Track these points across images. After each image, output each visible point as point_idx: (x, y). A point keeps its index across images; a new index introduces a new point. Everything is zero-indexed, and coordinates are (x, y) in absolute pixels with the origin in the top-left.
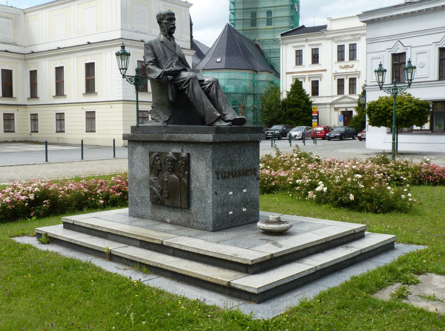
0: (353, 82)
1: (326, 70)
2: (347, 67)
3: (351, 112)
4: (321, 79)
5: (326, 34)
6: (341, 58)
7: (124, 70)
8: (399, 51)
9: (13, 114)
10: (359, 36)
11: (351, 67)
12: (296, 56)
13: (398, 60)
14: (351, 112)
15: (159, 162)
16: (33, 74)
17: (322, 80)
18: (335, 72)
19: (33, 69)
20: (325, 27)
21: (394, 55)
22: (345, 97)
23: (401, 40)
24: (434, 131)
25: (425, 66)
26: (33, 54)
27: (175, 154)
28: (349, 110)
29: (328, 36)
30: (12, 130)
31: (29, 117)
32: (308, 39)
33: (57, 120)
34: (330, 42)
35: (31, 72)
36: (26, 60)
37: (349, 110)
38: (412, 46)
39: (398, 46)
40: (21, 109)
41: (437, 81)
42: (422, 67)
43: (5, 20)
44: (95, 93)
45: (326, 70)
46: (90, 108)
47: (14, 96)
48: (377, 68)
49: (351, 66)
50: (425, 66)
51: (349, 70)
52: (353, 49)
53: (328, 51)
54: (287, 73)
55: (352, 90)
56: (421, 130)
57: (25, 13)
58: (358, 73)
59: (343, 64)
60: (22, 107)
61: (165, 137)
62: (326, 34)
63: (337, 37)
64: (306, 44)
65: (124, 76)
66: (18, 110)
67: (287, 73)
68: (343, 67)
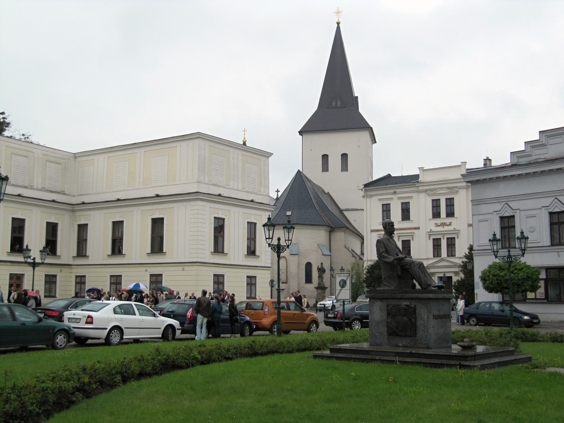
0: (451, 243)
1: (419, 228)
2: (443, 224)
3: (450, 278)
4: (413, 238)
5: (418, 186)
6: (436, 214)
7: (270, 240)
8: (507, 214)
9: (55, 276)
10: (457, 189)
11: (448, 225)
12: (383, 211)
13: (507, 223)
14: (450, 278)
15: (394, 311)
16: (82, 229)
17: (415, 238)
18: (429, 231)
19: (83, 222)
20: (417, 176)
21: (502, 218)
22: (443, 260)
23: (509, 203)
24: (550, 299)
25: (535, 227)
26: (82, 205)
27: (406, 305)
28: (448, 275)
29: (420, 188)
30: (53, 294)
31: (74, 279)
32: (397, 191)
33: (111, 283)
34: (423, 195)
35: (114, 223)
36: (73, 211)
37: (448, 275)
38: (521, 208)
39: (506, 209)
40: (65, 269)
41: (549, 246)
42: (532, 232)
43: (54, 165)
44: (163, 252)
45: (419, 228)
46: (116, 271)
47: (58, 253)
48: (491, 237)
49: (448, 224)
50: (535, 227)
51: (447, 228)
52: (450, 203)
53: (421, 206)
54: (372, 231)
55: (451, 251)
56: (536, 299)
57: (75, 158)
58: (457, 232)
59: (438, 221)
60: (67, 267)
61: (399, 296)
62: (418, 186)
63: (432, 190)
64: (395, 197)
65: (269, 245)
66: (61, 271)
67: (372, 231)
68: (439, 224)
